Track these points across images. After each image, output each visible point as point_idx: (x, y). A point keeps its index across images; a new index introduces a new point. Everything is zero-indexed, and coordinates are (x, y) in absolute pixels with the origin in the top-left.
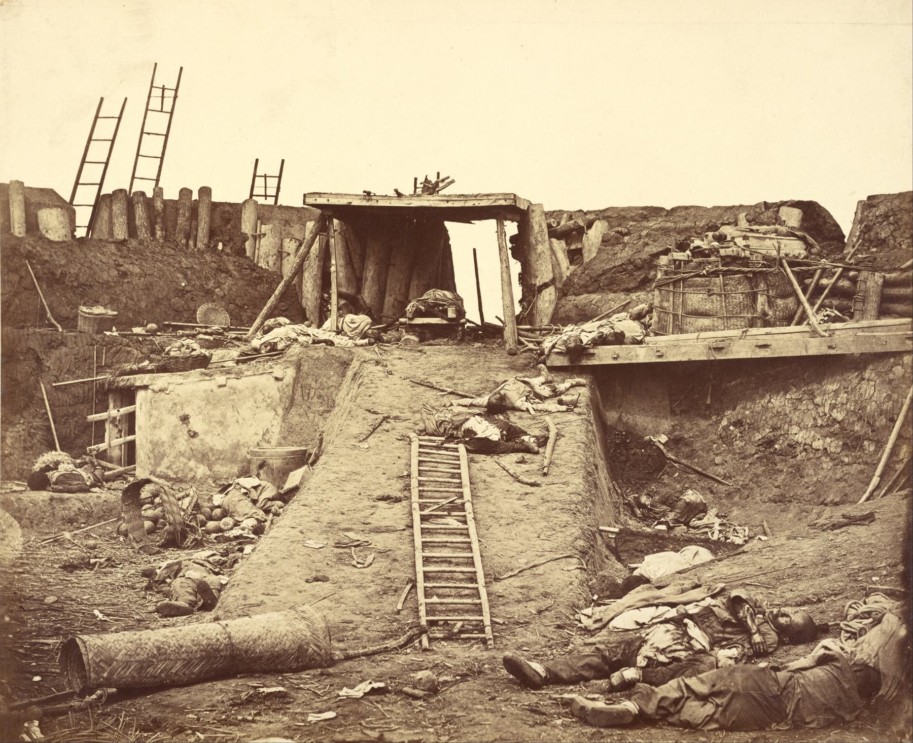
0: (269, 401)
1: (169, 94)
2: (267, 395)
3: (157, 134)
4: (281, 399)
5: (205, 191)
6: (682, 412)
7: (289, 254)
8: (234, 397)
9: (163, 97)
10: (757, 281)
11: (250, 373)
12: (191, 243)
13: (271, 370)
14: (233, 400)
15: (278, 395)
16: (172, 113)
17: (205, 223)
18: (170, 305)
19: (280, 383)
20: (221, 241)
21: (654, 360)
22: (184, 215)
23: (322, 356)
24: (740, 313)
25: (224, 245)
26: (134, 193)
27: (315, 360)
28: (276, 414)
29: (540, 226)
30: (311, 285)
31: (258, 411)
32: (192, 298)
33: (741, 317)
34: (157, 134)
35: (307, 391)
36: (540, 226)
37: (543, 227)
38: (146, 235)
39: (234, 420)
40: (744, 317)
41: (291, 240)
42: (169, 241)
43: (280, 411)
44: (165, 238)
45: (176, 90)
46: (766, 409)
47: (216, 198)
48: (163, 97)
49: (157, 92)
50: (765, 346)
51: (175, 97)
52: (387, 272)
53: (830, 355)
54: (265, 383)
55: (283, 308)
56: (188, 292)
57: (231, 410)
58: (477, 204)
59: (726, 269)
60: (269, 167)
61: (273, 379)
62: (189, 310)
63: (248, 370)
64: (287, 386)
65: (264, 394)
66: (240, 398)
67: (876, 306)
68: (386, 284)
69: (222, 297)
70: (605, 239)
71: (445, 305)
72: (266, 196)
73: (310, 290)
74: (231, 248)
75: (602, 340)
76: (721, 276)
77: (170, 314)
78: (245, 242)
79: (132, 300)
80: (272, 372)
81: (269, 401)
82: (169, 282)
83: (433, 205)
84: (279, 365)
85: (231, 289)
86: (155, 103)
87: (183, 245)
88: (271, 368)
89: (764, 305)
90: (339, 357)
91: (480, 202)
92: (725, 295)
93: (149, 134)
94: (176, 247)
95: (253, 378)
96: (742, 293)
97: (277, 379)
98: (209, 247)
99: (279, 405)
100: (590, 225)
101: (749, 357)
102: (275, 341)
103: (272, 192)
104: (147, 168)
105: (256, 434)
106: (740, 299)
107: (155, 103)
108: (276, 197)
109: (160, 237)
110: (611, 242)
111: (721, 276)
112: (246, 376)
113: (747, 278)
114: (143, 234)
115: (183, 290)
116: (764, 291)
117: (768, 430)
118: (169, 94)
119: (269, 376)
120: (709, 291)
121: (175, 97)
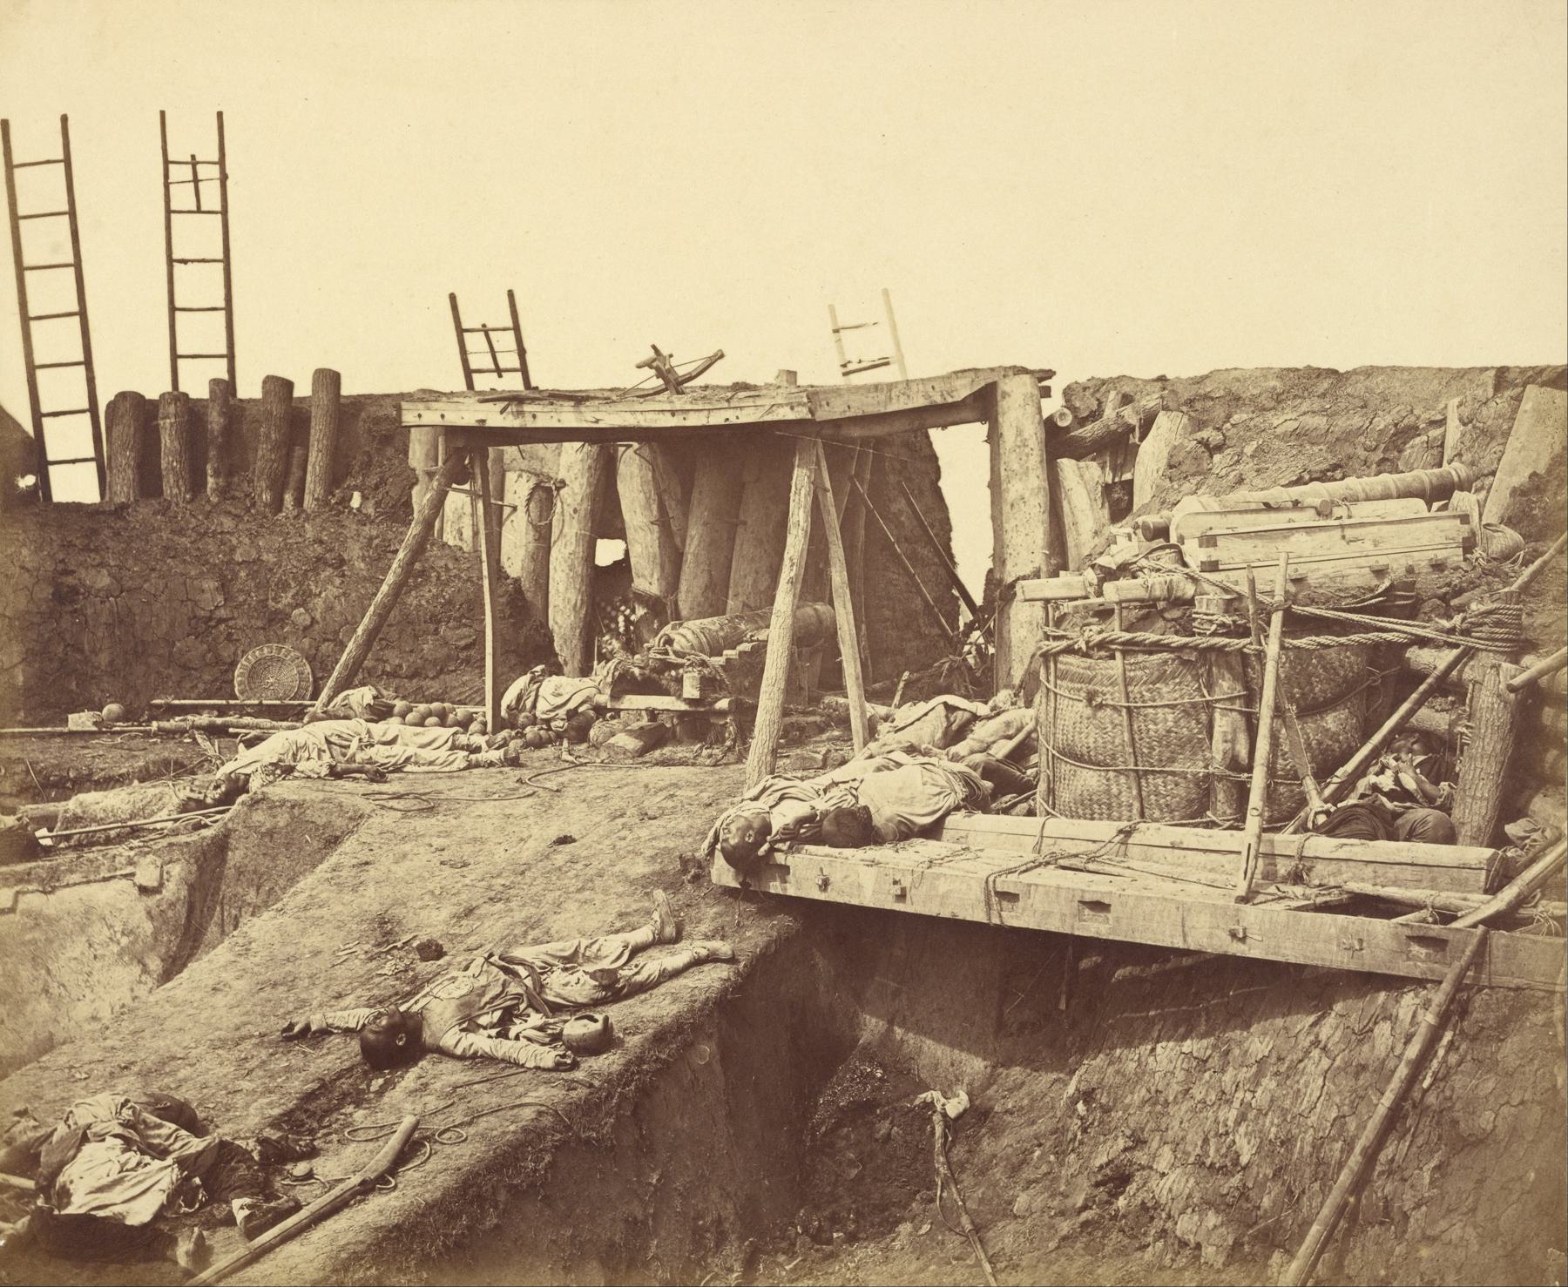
0: (124, 941)
1: (209, 172)
2: (119, 927)
3: (203, 261)
4: (156, 935)
5: (329, 379)
6: (1022, 1026)
7: (515, 509)
8: (37, 934)
9: (196, 181)
10: (1210, 672)
11: (76, 877)
12: (288, 498)
13: (129, 870)
14: (34, 942)
15: (148, 927)
16: (224, 212)
17: (319, 451)
18: (171, 653)
19: (152, 901)
20: (356, 488)
21: (891, 904)
22: (268, 436)
23: (281, 824)
24: (1172, 760)
25: (364, 498)
26: (112, 407)
27: (263, 835)
28: (145, 970)
29: (1019, 433)
30: (563, 575)
31: (98, 965)
32: (230, 634)
33: (1173, 774)
34: (203, 261)
35: (234, 912)
36: (1019, 433)
37: (1026, 435)
38: (175, 491)
39: (38, 986)
40: (1184, 775)
41: (520, 476)
42: (234, 498)
43: (155, 964)
44: (223, 492)
45: (222, 162)
46: (1142, 1072)
47: (349, 389)
48: (196, 181)
49: (180, 173)
50: (1099, 906)
51: (224, 178)
52: (732, 539)
53: (1235, 958)
54: (115, 897)
55: (462, 643)
56: (221, 621)
57: (29, 965)
58: (733, 420)
59: (1127, 636)
60: (485, 309)
61: (136, 891)
62: (218, 660)
63: (72, 872)
64: (172, 905)
65: (110, 927)
66: (51, 935)
67: (1493, 769)
68: (730, 567)
69: (306, 628)
70: (1175, 460)
71: (682, 666)
72: (499, 371)
73: (561, 588)
74: (378, 504)
75: (810, 831)
76: (1118, 655)
77: (169, 677)
78: (411, 488)
79: (81, 651)
80: (133, 874)
81: (124, 941)
82: (176, 604)
83: (644, 424)
84: (150, 857)
85: (332, 608)
86: (183, 197)
87: (266, 505)
88: (131, 862)
89: (1234, 741)
90: (325, 827)
91: (738, 412)
92: (1128, 708)
93: (185, 262)
94: (248, 510)
95: (85, 889)
96: (1172, 707)
97: (144, 890)
98: (327, 503)
99: (152, 949)
100: (1147, 423)
101: (1068, 931)
102: (248, 771)
103: (509, 360)
104: (200, 333)
105: (94, 1018)
106: (1166, 720)
107: (183, 197)
108: (524, 370)
109: (214, 490)
110: (1184, 468)
111: (1118, 655)
112: (68, 885)
113: (1185, 663)
114: (171, 487)
115: (210, 619)
116: (1231, 700)
117: (1121, 1143)
118: (209, 172)
119: (125, 883)
120: (1091, 697)
121: (224, 178)
